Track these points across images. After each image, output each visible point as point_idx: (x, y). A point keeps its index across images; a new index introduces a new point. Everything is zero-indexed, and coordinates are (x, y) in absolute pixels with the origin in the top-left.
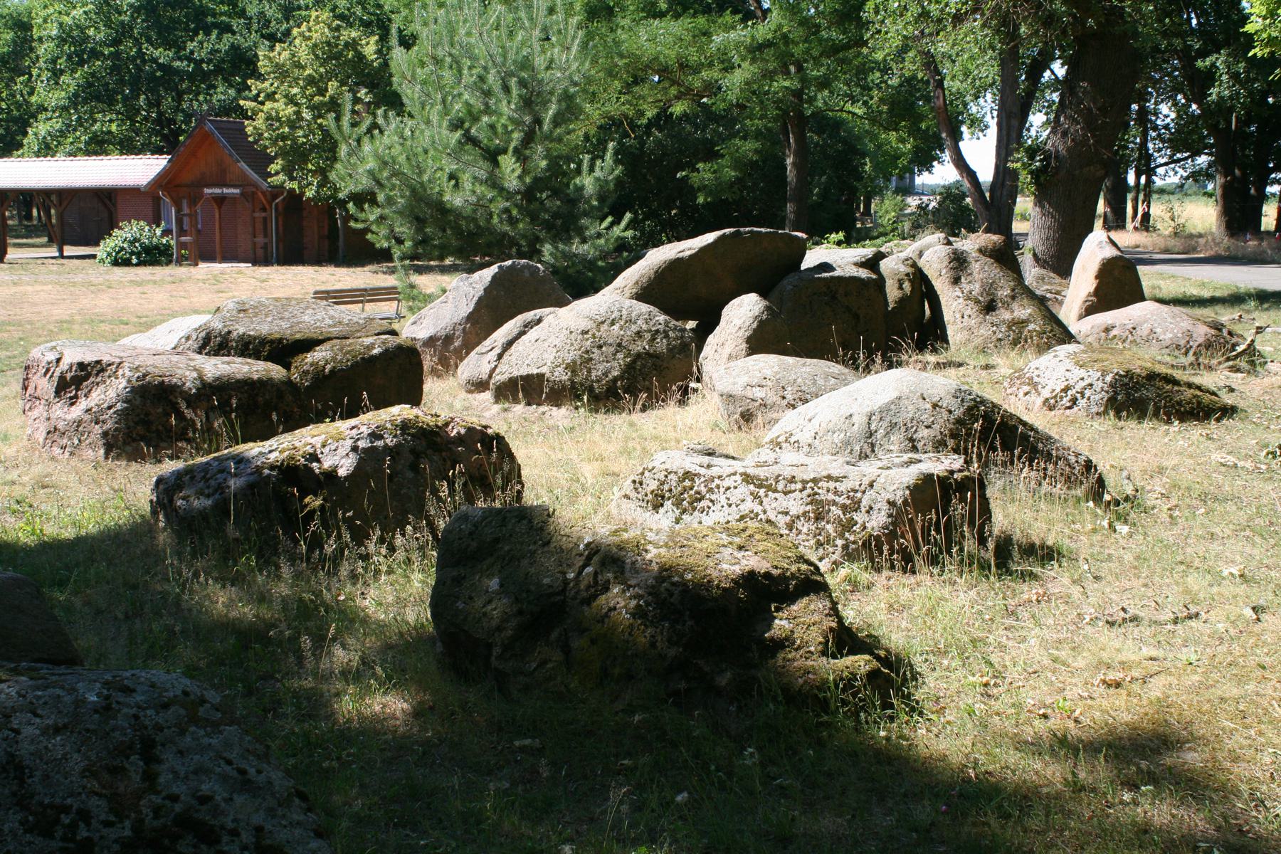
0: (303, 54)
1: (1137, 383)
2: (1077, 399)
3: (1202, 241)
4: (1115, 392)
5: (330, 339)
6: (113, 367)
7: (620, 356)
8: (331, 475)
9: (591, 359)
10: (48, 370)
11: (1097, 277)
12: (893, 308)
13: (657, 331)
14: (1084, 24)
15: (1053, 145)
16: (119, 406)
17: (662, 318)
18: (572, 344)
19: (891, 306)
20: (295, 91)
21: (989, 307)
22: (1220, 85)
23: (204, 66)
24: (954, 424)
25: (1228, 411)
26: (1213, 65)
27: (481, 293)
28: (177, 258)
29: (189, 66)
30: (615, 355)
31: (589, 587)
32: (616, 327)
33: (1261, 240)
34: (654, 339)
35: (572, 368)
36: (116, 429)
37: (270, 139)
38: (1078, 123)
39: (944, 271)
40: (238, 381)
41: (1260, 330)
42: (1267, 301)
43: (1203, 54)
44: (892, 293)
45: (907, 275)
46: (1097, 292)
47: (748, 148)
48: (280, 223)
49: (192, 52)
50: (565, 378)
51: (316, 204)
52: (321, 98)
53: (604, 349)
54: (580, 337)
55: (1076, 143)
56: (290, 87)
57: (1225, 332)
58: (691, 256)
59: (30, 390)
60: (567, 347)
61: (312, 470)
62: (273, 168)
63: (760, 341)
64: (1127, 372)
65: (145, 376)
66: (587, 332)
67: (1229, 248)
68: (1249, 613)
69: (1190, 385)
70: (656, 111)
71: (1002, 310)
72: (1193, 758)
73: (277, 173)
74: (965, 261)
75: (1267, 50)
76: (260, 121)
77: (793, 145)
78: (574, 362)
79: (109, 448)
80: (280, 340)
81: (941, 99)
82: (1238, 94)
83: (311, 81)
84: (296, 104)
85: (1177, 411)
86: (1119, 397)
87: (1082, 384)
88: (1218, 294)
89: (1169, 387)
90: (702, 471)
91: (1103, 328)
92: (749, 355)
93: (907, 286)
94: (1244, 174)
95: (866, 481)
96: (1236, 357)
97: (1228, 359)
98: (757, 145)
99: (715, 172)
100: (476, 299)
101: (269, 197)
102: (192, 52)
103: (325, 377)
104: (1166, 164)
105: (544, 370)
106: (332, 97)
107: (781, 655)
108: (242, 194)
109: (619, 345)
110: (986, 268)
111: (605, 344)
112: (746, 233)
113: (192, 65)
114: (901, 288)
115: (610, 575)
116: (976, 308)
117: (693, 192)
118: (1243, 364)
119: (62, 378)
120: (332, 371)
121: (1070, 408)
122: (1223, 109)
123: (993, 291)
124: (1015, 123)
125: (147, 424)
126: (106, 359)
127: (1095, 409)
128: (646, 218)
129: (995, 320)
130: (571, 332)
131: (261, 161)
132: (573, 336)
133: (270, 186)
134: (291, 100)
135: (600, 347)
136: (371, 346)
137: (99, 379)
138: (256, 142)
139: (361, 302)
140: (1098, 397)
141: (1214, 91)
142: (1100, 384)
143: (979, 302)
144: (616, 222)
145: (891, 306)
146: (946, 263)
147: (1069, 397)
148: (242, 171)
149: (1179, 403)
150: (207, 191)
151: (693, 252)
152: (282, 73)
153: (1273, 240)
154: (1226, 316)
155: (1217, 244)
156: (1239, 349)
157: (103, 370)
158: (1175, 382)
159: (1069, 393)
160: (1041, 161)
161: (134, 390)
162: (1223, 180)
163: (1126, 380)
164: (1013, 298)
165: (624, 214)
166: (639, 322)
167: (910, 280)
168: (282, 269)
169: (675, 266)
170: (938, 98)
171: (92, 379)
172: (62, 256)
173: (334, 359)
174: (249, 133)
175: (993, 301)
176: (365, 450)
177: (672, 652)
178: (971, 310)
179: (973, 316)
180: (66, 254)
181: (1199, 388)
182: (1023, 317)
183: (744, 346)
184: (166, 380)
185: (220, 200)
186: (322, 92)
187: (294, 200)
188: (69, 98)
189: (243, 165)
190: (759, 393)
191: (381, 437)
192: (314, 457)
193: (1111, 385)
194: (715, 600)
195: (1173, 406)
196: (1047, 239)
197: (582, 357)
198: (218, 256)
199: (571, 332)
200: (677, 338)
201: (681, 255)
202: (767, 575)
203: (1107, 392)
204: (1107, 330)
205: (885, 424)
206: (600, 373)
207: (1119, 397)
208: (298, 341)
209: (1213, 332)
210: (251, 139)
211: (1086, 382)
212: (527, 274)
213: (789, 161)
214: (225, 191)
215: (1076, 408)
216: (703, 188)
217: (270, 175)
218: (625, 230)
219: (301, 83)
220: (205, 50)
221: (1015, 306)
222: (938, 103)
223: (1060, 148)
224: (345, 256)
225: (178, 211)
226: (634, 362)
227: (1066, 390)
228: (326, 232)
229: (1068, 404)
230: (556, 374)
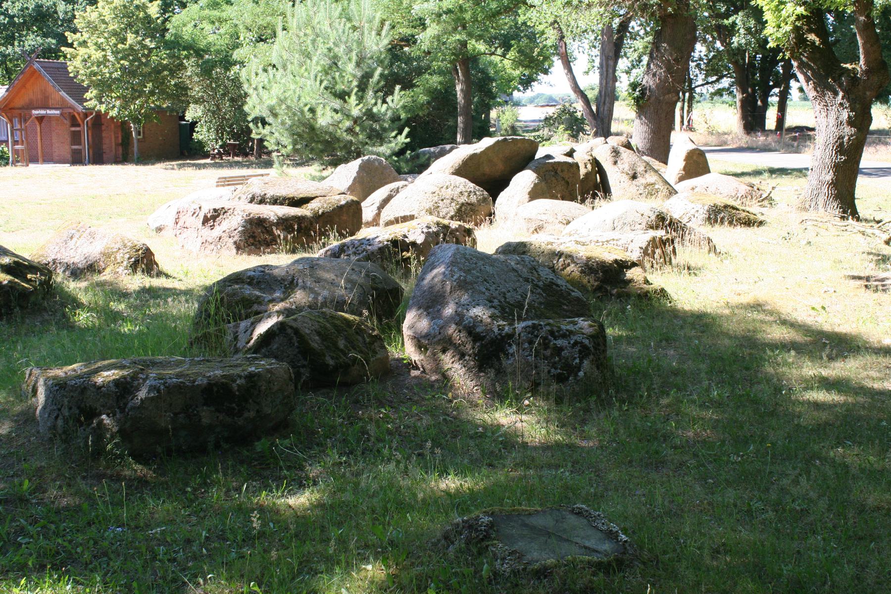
0: (108, 15)
3: (730, 138)
4: (710, 214)
5: (317, 197)
6: (231, 210)
7: (453, 204)
8: (414, 244)
9: (439, 207)
10: (194, 213)
11: (684, 160)
13: (470, 192)
14: (666, 10)
15: (647, 82)
16: (240, 229)
17: (472, 185)
20: (102, 40)
21: (634, 177)
22: (739, 36)
23: (16, 19)
25: (761, 223)
26: (734, 24)
27: (355, 174)
28: (13, 161)
29: (4, 20)
31: (562, 265)
32: (449, 189)
33: (767, 136)
36: (240, 240)
37: (86, 75)
38: (662, 69)
39: (608, 158)
40: (293, 216)
41: (773, 188)
42: (775, 174)
43: (727, 15)
44: (583, 171)
45: (589, 160)
46: (685, 169)
47: (435, 80)
48: (90, 134)
49: (7, 10)
51: (118, 120)
52: (123, 46)
54: (431, 195)
55: (661, 81)
56: (98, 37)
57: (755, 188)
58: (481, 152)
59: (180, 223)
60: (425, 201)
61: (405, 241)
62: (88, 95)
63: (535, 194)
65: (250, 214)
67: (747, 142)
68: (781, 278)
69: (744, 211)
71: (641, 178)
72: (768, 307)
73: (91, 99)
74: (619, 152)
75: (776, 44)
76: (77, 62)
78: (430, 208)
79: (238, 248)
80: (293, 198)
81: (564, 48)
82: (750, 42)
83: (115, 34)
84: (103, 50)
88: (745, 170)
89: (735, 211)
90: (556, 241)
91: (691, 188)
92: (530, 201)
93: (589, 167)
94: (754, 91)
95: (629, 240)
96: (763, 200)
97: (759, 202)
98: (441, 79)
99: (413, 96)
101: (82, 115)
102: (7, 10)
103: (320, 216)
104: (702, 85)
106: (131, 45)
107: (630, 284)
108: (62, 114)
109: (452, 199)
113: (7, 19)
114: (586, 167)
115: (569, 261)
118: (766, 203)
119: (205, 217)
120: (323, 213)
122: (740, 51)
124: (611, 63)
125: (254, 237)
126: (226, 207)
129: (638, 184)
131: (78, 91)
132: (426, 195)
133: (86, 109)
134: (99, 47)
135: (442, 200)
136: (339, 201)
137: (225, 216)
138: (75, 77)
139: (242, 184)
141: (735, 40)
143: (628, 174)
145: (581, 177)
148: (62, 98)
150: (35, 112)
152: (93, 28)
153: (775, 136)
154: (755, 181)
155: (739, 139)
156: (764, 196)
157: (226, 212)
158: (737, 209)
160: (639, 91)
161: (246, 221)
162: (741, 96)
163: (714, 208)
164: (646, 171)
168: (141, 169)
170: (561, 47)
171: (221, 217)
173: (322, 207)
174: (70, 71)
175: (635, 173)
176: (427, 233)
177: (596, 284)
178: (625, 178)
181: (748, 212)
182: (653, 182)
183: (528, 196)
184: (261, 216)
185: (41, 119)
186: (123, 40)
187: (99, 118)
189: (63, 93)
190: (544, 217)
191: (430, 228)
192: (405, 236)
193: (708, 211)
194: (607, 267)
196: (645, 139)
198: (40, 159)
200: (481, 195)
201: (475, 152)
202: (621, 260)
205: (621, 223)
208: (302, 198)
209: (750, 188)
210: (71, 75)
212: (377, 164)
213: (459, 88)
214: (49, 112)
217: (86, 101)
219: (106, 35)
220: (17, 8)
221: (647, 175)
222: (561, 50)
223: (651, 83)
224: (138, 158)
225: (12, 127)
226: (461, 207)
228: (120, 141)
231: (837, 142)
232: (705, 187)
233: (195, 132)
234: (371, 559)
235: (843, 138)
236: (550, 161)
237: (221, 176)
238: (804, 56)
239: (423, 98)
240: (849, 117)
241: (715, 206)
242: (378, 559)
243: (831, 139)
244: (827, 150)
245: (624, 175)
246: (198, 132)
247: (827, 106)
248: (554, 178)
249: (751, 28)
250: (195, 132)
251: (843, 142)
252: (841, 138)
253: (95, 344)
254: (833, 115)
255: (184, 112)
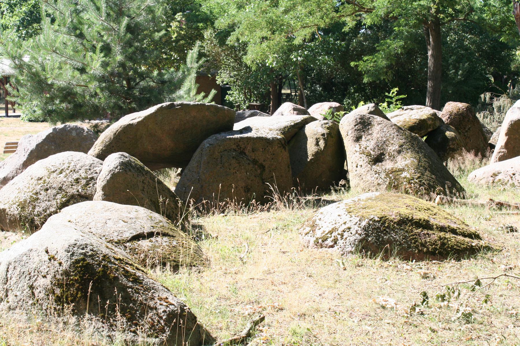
1: (388, 227)
2: (337, 240)
4: (367, 235)
7: (59, 196)
9: (38, 199)
12: (311, 159)
18: (29, 188)
19: (310, 157)
24: (62, 275)
30: (56, 195)
34: (88, 185)
35: (23, 206)
39: (350, 132)
45: (323, 135)
50: (16, 212)
53: (49, 191)
58: (138, 122)
64: (381, 218)
66: (41, 179)
70: (355, 23)
71: (388, 161)
77: (432, 42)
78: (25, 201)
85: (420, 251)
86: (370, 239)
87: (344, 227)
91: (491, 174)
100: (29, 151)
105: (6, 207)
109: (60, 189)
110: (385, 129)
111: (50, 187)
112: (178, 105)
114: (317, 144)
116: (366, 159)
117: (360, 75)
121: (332, 247)
123: (385, 146)
127: (349, 249)
128: (355, 92)
130: (32, 179)
140: (352, 239)
142: (356, 228)
144: (206, 97)
145: (310, 157)
146: (353, 126)
147: (333, 238)
149: (423, 245)
151: (140, 119)
159: (333, 235)
165: (211, 91)
166: (81, 172)
167: (324, 139)
169: (129, 127)
172: (7, 116)
175: (382, 154)
179: (363, 167)
180: (9, 115)
188: (20, 21)
193: (365, 229)
195: (417, 247)
197: (31, 197)
199: (32, 179)
201: (131, 122)
203: (360, 235)
204: (495, 175)
206: (41, 209)
207: (370, 239)
211: (347, 226)
212: (74, 134)
215: (336, 247)
216: (368, 72)
218: (212, 101)
221: (399, 158)
227: (331, 232)
229: (331, 244)
230: (12, 210)
232: (511, 173)
233: (227, 94)
236: (249, 135)
237: (9, 141)
239: (383, 63)
241: (383, 220)
245: (364, 157)
246: (230, 94)
248: (234, 161)
250: (227, 94)
253: (74, 292)
255: (214, 76)
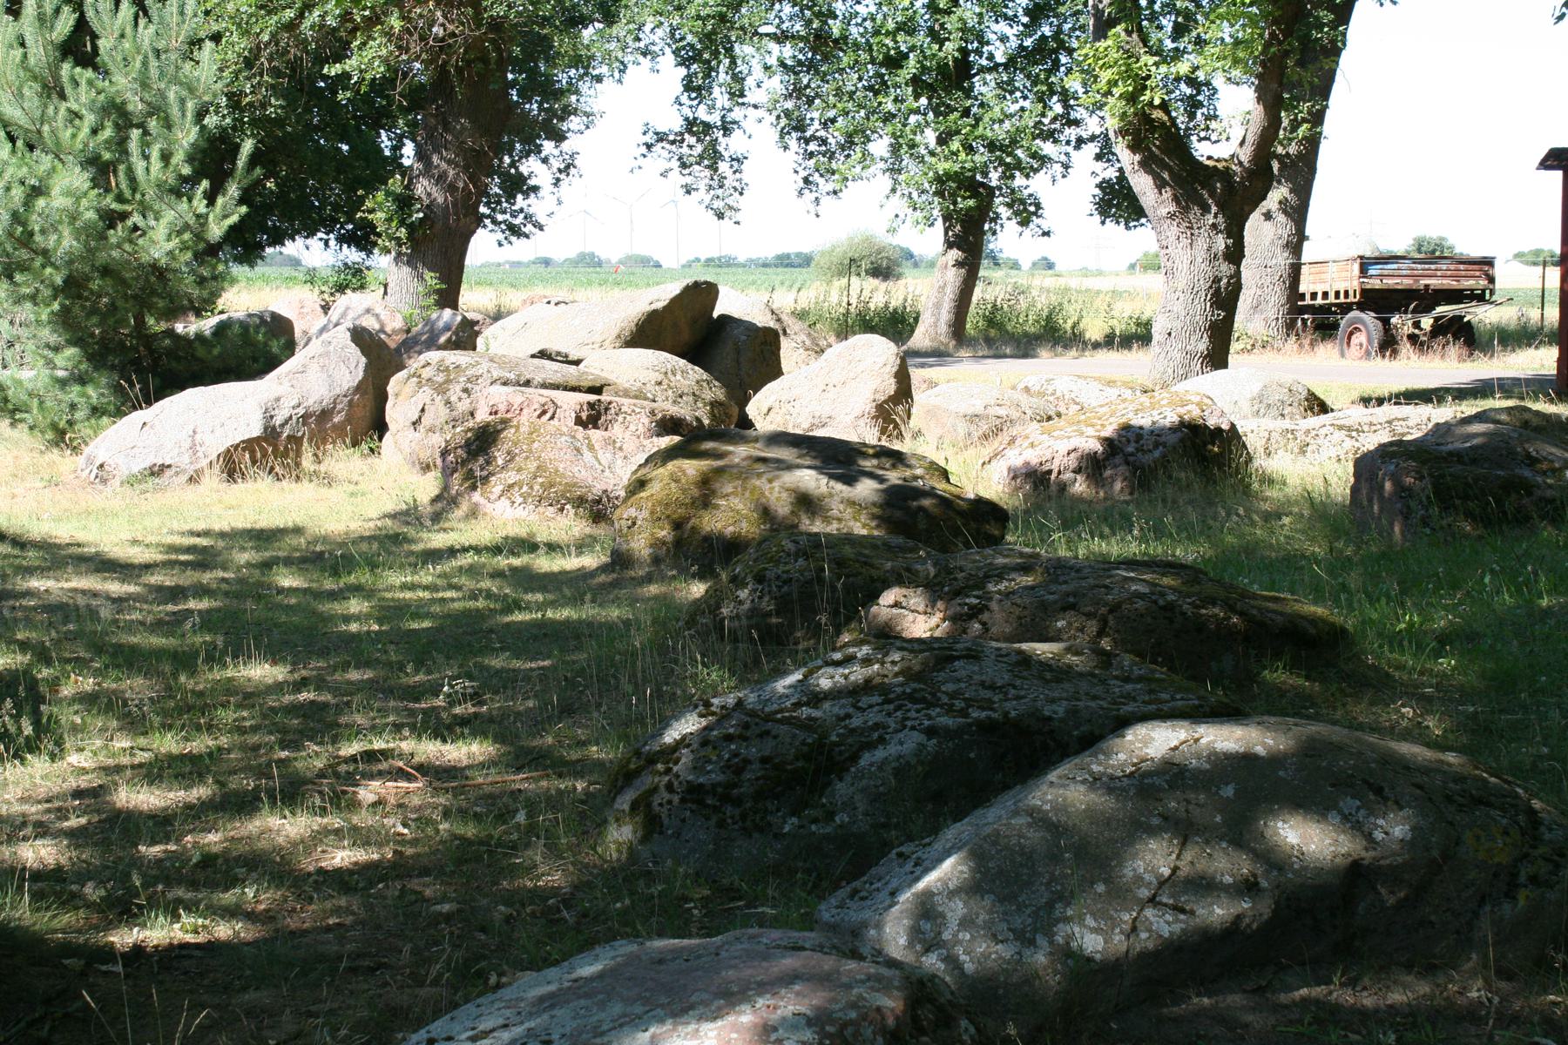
58: (664, 307)
201: (654, 307)
231: (1211, 287)
234: (312, 688)
235: (1220, 280)
238: (1154, 145)
240: (1227, 247)
242: (101, 217)
243: (1202, 282)
244: (1197, 301)
247: (1191, 228)
249: (242, 93)
251: (1219, 288)
252: (1217, 280)
254: (1202, 243)
